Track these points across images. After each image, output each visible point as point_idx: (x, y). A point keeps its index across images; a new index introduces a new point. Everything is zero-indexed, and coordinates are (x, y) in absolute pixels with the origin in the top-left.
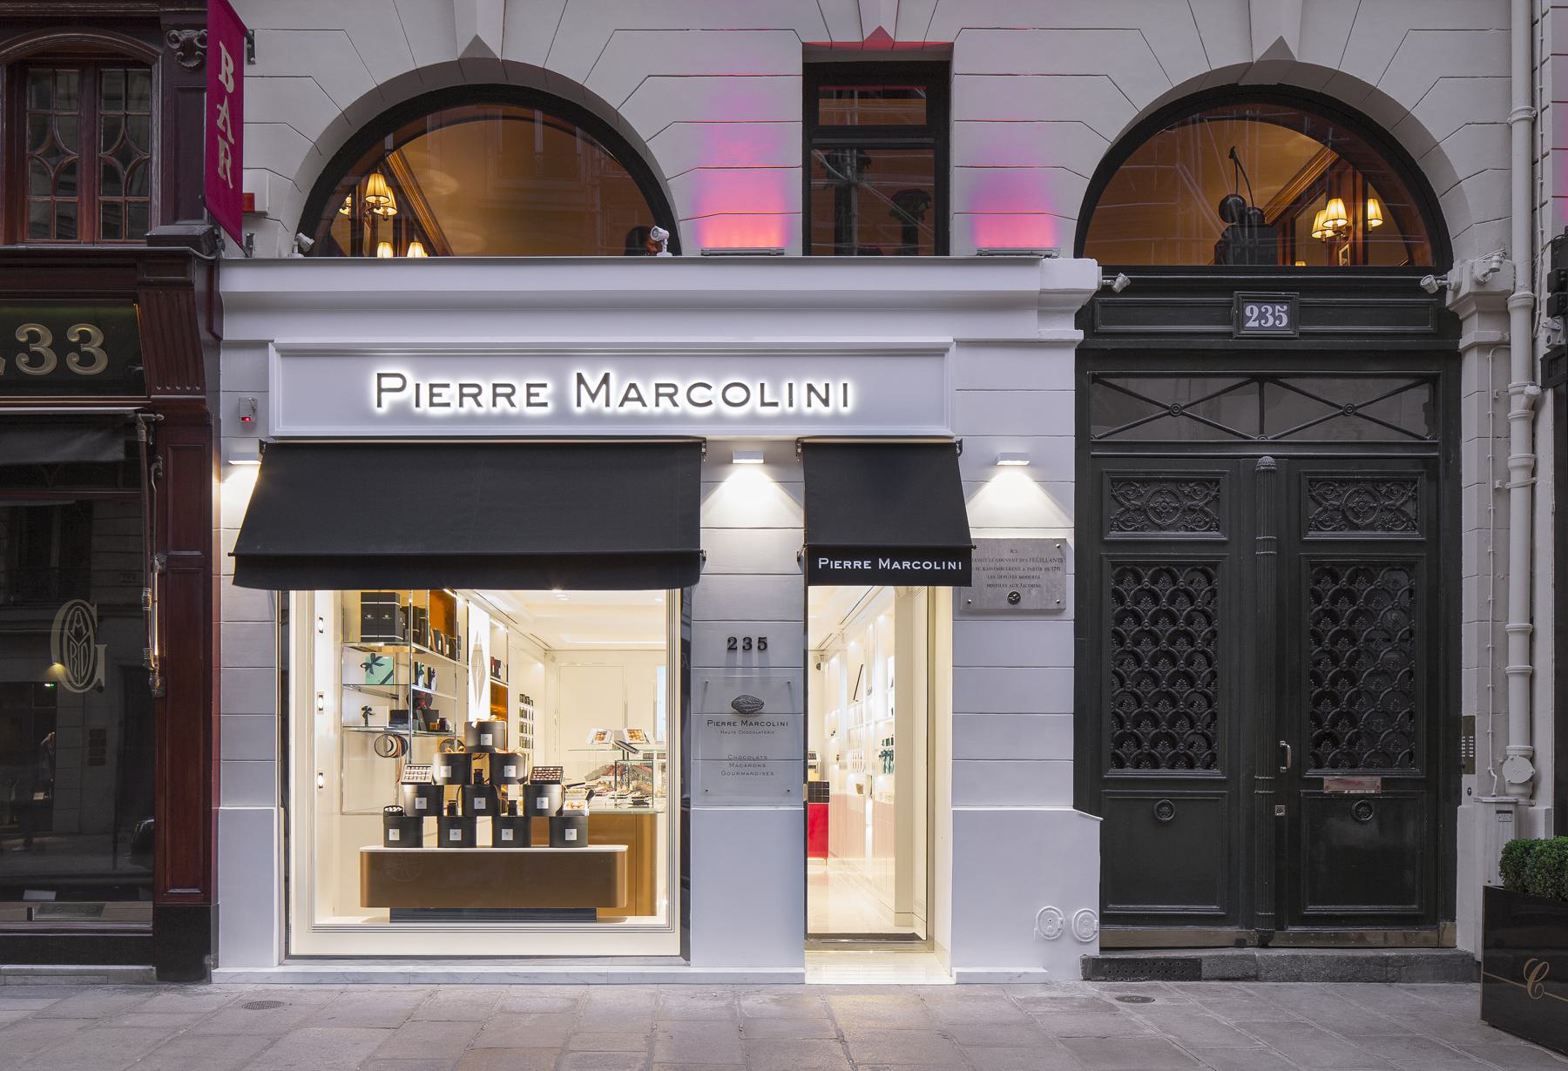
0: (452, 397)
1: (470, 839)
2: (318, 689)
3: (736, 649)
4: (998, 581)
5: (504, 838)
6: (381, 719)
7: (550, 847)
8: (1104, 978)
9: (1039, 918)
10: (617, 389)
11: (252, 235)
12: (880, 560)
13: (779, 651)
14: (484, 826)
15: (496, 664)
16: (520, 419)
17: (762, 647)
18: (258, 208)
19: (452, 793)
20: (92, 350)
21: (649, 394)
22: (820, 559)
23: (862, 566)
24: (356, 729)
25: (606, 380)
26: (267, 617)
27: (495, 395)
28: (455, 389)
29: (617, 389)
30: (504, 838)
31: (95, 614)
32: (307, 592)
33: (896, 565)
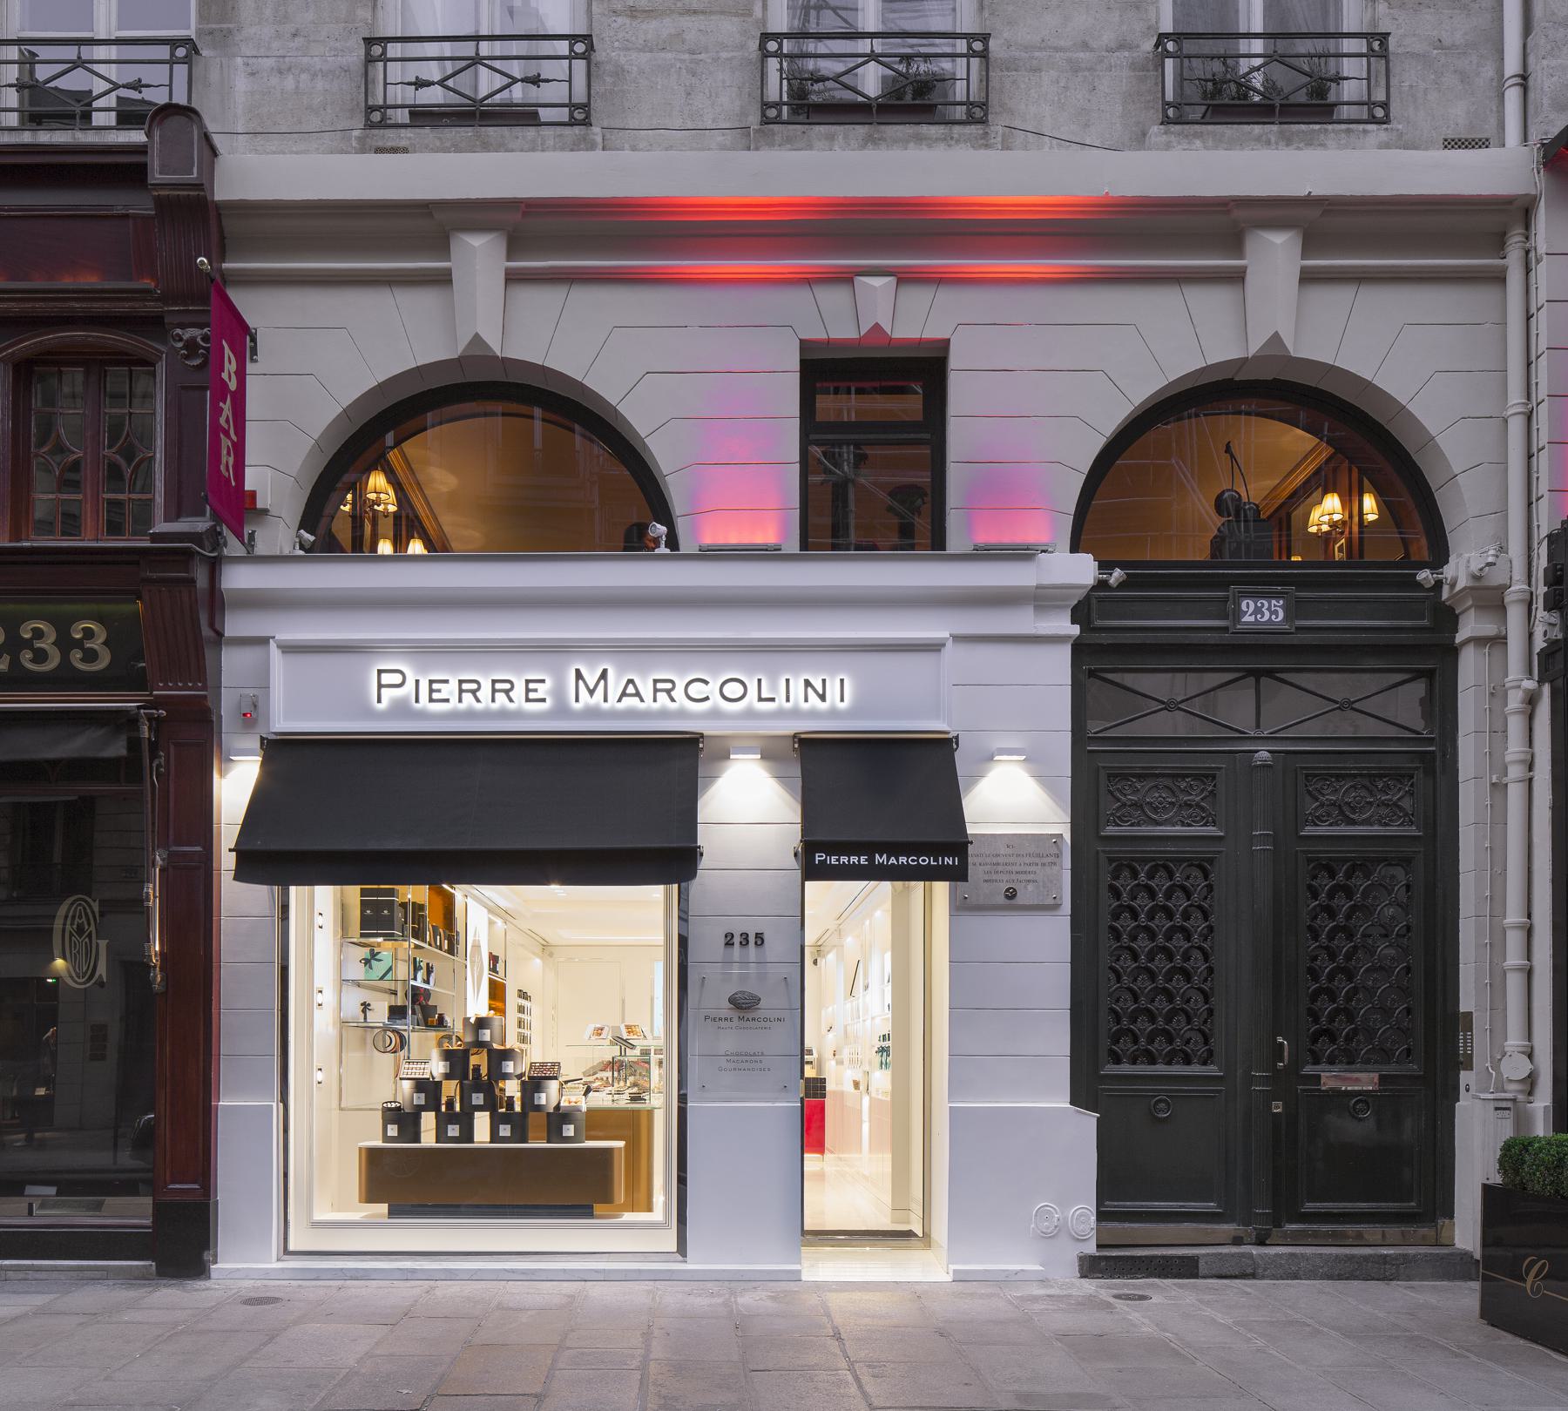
0: (451, 693)
1: (467, 1135)
3: (733, 944)
4: (995, 877)
7: (548, 1143)
8: (1100, 1276)
9: (1036, 1215)
10: (615, 685)
11: (254, 532)
12: (877, 856)
13: (776, 946)
14: (482, 1122)
15: (494, 959)
16: (519, 715)
17: (759, 942)
18: (260, 505)
19: (450, 1089)
20: (95, 647)
21: (646, 690)
22: (817, 855)
23: (859, 861)
24: (355, 1025)
25: (604, 675)
26: (267, 912)
27: (494, 691)
29: (615, 685)
31: (96, 909)
32: (306, 887)
33: (893, 861)
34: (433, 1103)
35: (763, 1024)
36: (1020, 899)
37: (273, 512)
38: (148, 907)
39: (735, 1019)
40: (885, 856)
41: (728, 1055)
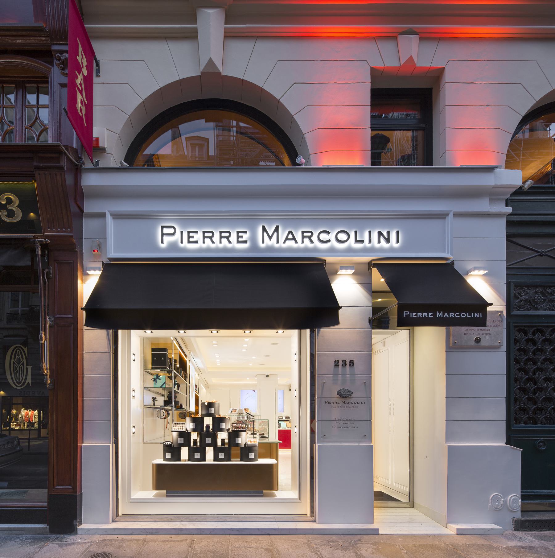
0: (199, 238)
1: (203, 458)
2: (132, 387)
3: (339, 366)
4: (470, 332)
5: (220, 457)
6: (160, 401)
7: (241, 460)
8: (526, 530)
9: (491, 499)
10: (283, 234)
11: (98, 161)
12: (438, 313)
13: (359, 367)
14: (210, 452)
15: (196, 386)
16: (233, 250)
17: (351, 365)
18: (101, 145)
19: (194, 436)
20: (14, 209)
21: (298, 236)
22: (405, 312)
23: (428, 315)
24: (149, 407)
25: (277, 229)
26: (107, 350)
27: (221, 237)
28: (200, 234)
29: (283, 234)
30: (220, 457)
31: (26, 352)
32: (127, 330)
33: (446, 315)
34: (187, 443)
35: (354, 405)
36: (483, 343)
37: (108, 150)
38: (42, 344)
39: (340, 403)
40: (442, 313)
41: (336, 420)
